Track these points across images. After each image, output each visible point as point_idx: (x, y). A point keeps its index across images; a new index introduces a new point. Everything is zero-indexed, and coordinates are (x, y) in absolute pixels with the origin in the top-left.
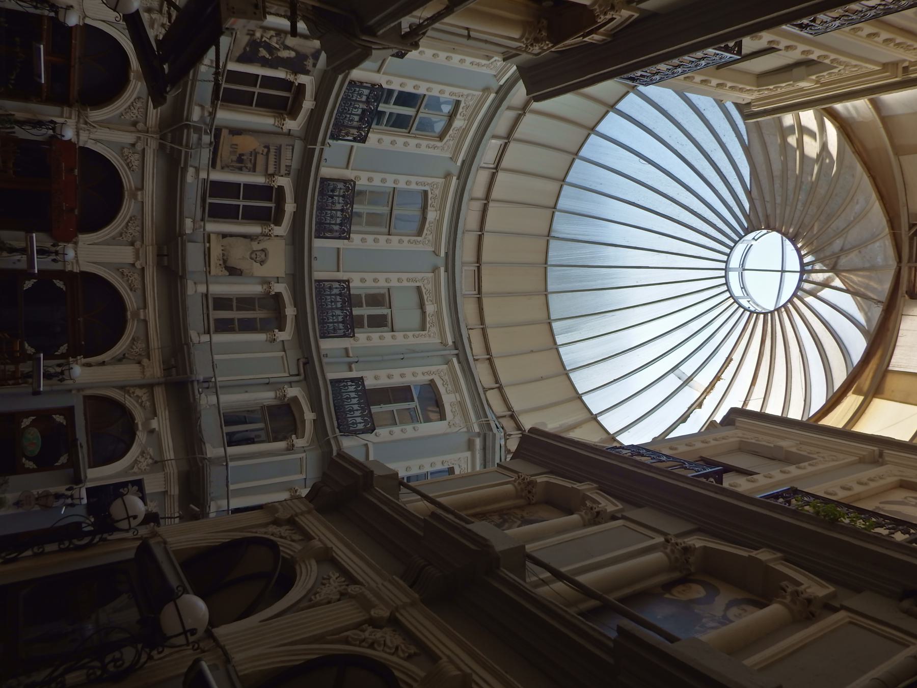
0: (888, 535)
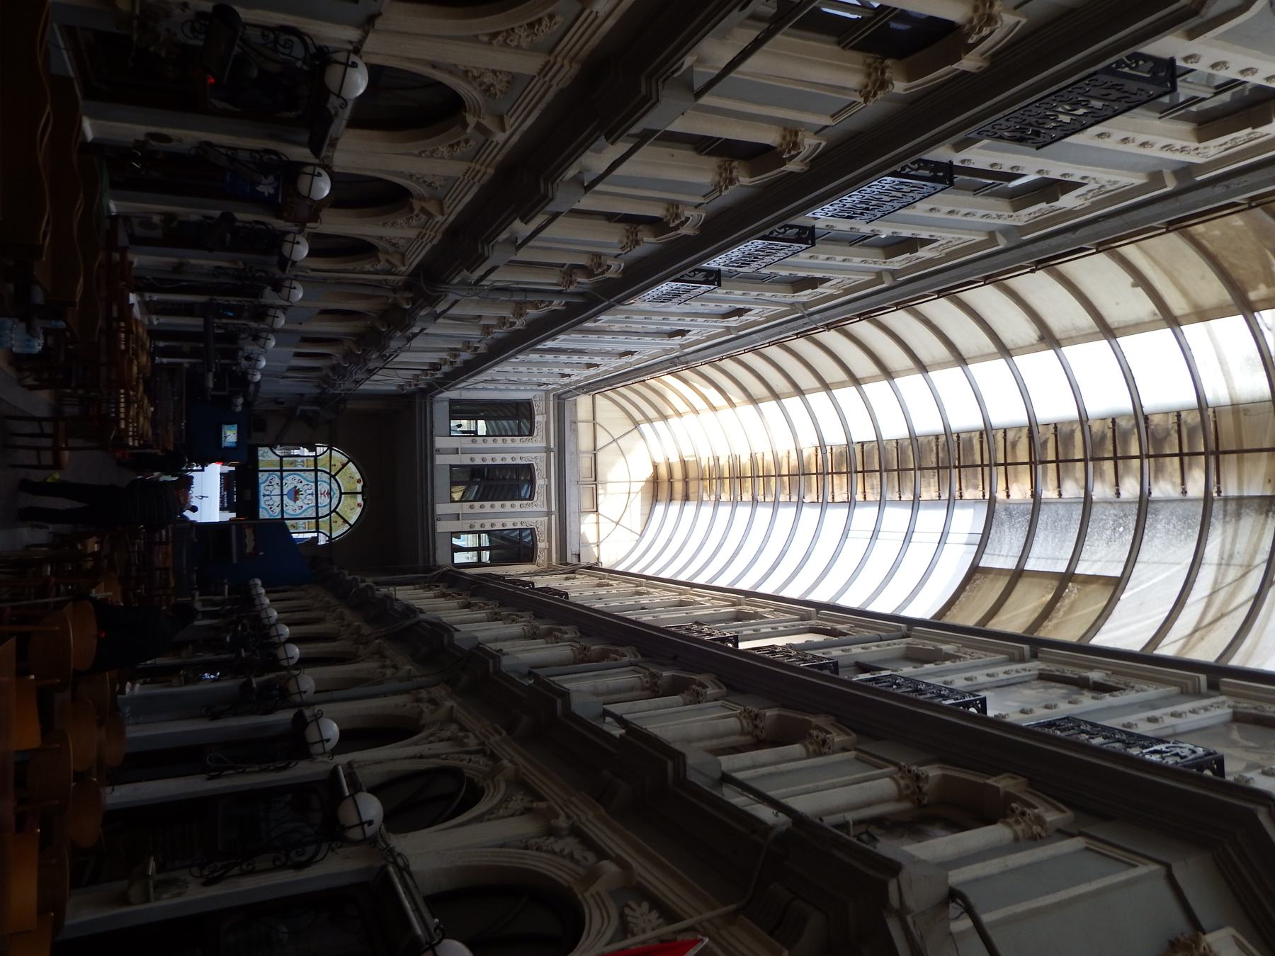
0: (1087, 740)
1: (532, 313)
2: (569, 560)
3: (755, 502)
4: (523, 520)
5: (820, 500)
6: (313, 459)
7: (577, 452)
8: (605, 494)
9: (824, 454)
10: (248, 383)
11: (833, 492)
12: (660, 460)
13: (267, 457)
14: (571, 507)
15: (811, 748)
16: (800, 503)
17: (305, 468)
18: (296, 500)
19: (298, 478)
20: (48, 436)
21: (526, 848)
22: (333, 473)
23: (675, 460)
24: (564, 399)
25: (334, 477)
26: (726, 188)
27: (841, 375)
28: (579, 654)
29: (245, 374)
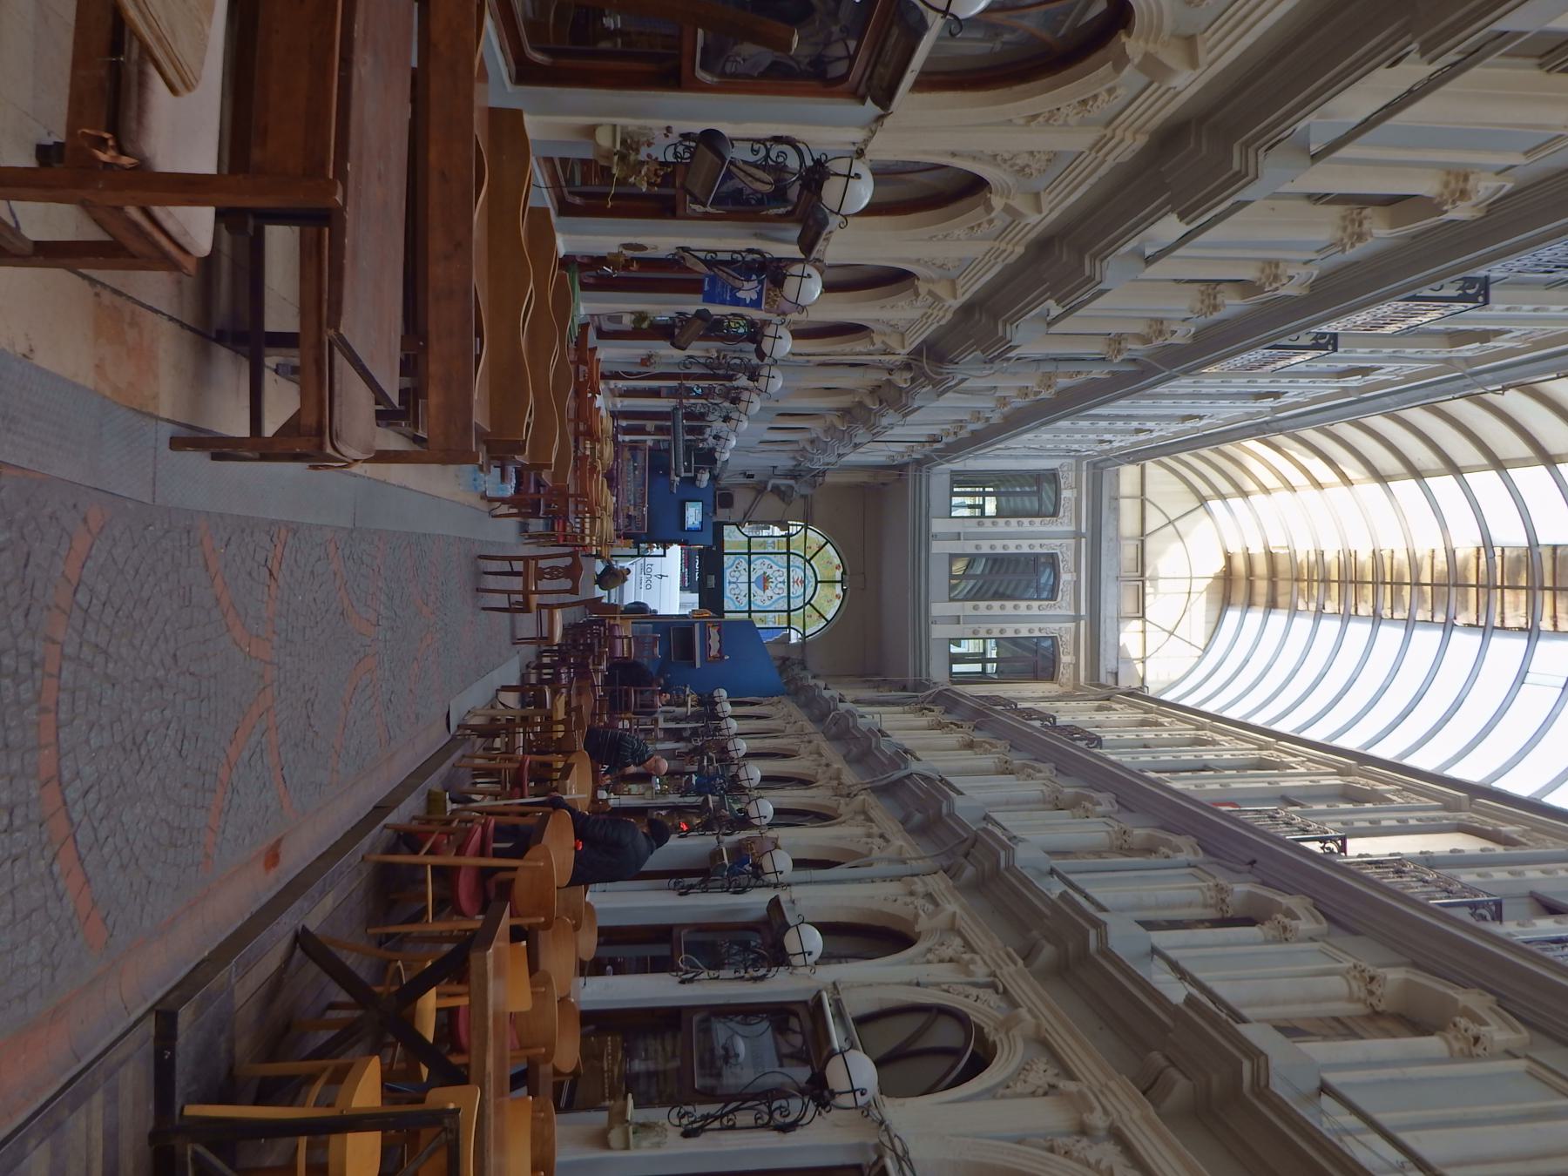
1: (1063, 382)
2: (1103, 680)
3: (1377, 618)
4: (1042, 625)
5: (1482, 623)
6: (785, 539)
7: (1118, 538)
8: (1155, 594)
9: (1490, 559)
10: (715, 461)
11: (1503, 612)
12: (1236, 549)
13: (733, 537)
14: (1108, 610)
15: (1457, 1046)
16: (1449, 625)
17: (776, 551)
18: (765, 588)
19: (767, 562)
20: (518, 574)
21: (1051, 1150)
22: (808, 558)
23: (1257, 550)
24: (1102, 469)
25: (809, 561)
26: (1353, 246)
27: (1522, 450)
28: (1117, 839)
29: (712, 450)
